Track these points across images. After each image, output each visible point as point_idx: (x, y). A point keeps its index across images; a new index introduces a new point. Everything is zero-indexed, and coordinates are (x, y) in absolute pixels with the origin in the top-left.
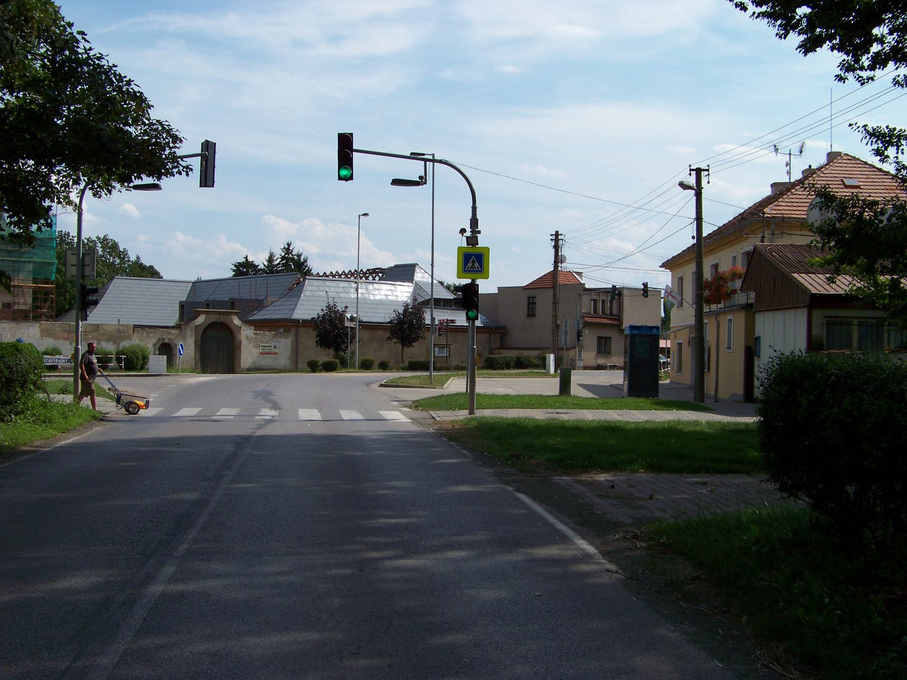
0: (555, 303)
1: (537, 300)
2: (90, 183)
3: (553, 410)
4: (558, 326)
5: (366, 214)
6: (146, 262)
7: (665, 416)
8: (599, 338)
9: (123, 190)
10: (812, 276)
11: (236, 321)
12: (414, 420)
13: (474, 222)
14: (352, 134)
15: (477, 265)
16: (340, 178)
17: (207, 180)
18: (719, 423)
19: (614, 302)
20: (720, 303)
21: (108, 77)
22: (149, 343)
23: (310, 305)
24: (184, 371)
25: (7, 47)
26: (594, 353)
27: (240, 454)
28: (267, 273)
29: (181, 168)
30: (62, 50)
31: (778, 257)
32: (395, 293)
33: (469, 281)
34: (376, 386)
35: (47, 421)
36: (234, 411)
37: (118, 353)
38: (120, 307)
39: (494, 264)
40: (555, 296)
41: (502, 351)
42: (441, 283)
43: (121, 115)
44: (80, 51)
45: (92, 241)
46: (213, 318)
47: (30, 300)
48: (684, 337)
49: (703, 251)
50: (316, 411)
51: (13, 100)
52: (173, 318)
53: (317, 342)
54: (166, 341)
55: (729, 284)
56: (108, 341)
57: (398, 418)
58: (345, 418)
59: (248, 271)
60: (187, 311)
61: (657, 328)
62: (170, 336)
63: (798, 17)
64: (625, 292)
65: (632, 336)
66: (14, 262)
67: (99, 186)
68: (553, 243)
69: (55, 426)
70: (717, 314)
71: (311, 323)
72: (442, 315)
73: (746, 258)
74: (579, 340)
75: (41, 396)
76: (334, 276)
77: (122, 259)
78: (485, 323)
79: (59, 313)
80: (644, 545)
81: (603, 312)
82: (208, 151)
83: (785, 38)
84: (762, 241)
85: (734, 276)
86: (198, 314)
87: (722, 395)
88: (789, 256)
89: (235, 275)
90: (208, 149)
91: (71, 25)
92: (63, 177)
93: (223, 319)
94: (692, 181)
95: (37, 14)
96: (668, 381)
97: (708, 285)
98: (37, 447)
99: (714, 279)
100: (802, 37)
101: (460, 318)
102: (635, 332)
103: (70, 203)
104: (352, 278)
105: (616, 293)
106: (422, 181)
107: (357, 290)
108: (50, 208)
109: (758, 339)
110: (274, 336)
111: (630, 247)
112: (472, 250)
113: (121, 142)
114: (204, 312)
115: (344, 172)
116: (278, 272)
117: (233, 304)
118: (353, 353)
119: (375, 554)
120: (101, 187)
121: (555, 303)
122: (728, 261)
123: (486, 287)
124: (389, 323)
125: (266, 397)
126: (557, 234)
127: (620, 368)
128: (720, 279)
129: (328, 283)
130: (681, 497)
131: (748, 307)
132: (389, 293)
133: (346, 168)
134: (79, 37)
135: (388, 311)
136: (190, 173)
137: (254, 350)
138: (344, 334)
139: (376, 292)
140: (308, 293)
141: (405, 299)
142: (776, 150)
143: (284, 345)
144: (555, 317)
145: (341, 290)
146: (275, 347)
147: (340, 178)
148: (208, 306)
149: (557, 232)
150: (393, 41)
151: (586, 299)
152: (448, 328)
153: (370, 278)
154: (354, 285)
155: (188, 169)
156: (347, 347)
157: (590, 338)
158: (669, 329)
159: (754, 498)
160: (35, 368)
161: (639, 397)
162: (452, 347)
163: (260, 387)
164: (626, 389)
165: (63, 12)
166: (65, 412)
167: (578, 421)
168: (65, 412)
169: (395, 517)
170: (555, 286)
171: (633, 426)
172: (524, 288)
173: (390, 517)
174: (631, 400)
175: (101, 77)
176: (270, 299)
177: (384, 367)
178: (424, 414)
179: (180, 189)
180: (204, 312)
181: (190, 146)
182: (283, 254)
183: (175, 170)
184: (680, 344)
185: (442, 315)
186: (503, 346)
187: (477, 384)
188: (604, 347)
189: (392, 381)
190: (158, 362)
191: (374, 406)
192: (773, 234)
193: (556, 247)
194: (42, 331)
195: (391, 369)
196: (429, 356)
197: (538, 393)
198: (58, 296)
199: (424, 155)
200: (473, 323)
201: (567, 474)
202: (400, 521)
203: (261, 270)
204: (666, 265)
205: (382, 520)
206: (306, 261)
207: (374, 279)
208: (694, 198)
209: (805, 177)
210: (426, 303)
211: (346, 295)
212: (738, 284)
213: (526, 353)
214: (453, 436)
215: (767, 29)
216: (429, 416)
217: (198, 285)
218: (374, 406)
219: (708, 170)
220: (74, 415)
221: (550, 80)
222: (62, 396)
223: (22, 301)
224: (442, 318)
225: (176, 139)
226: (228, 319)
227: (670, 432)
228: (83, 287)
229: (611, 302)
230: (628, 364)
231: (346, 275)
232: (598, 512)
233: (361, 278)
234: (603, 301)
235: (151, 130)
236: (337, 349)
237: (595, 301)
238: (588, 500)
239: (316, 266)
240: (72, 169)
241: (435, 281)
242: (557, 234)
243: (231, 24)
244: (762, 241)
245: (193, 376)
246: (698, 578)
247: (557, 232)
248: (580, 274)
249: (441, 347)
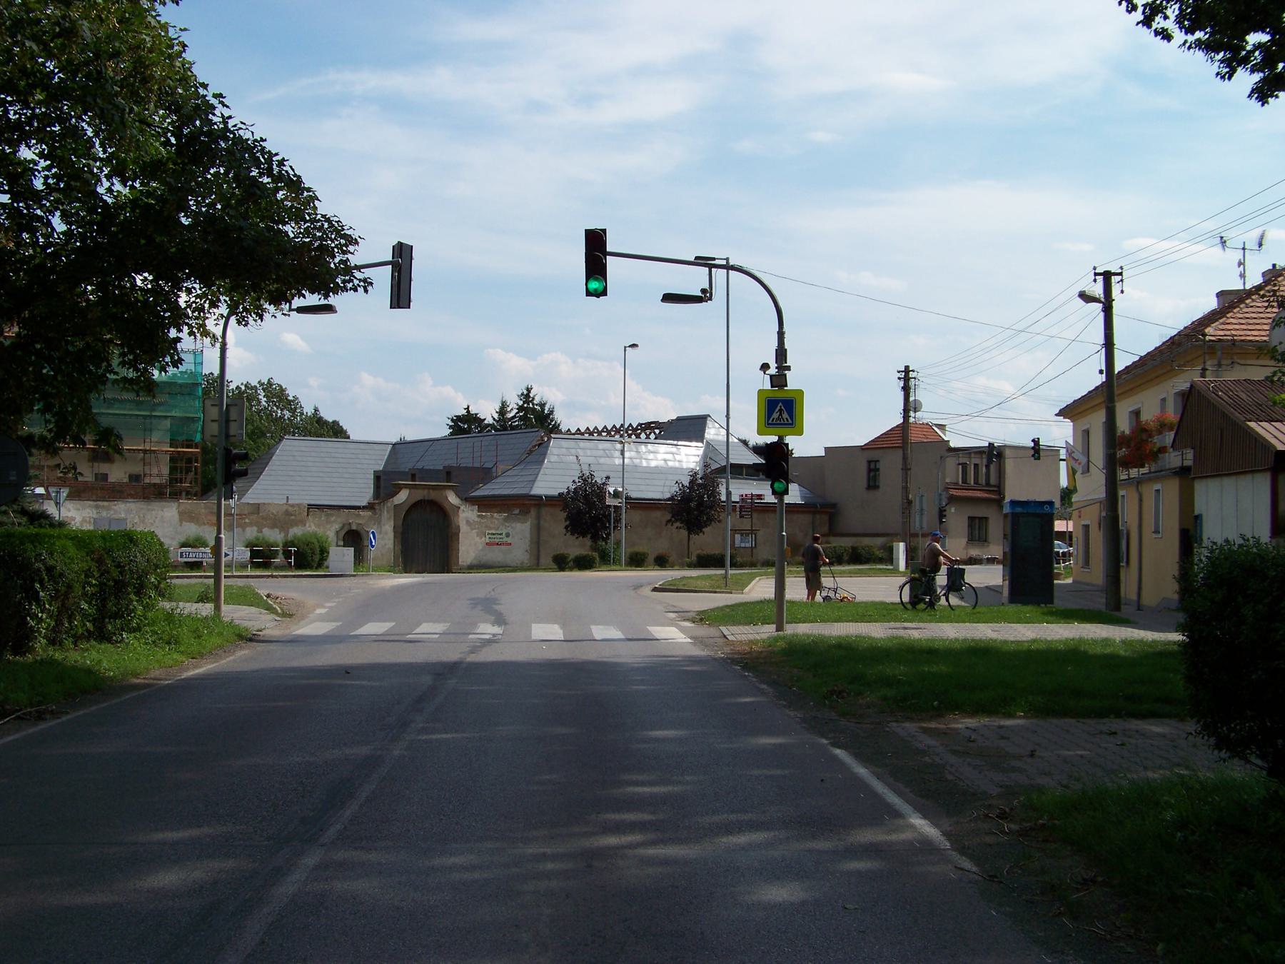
0: (906, 469)
1: (881, 465)
2: (233, 310)
3: (898, 625)
4: (910, 502)
5: (634, 346)
6: (328, 416)
7: (1061, 631)
8: (971, 519)
9: (279, 314)
10: (1277, 424)
11: (453, 499)
12: (697, 640)
13: (781, 354)
14: (604, 231)
15: (785, 415)
16: (589, 293)
17: (400, 297)
18: (1141, 641)
19: (992, 467)
20: (1143, 466)
21: (253, 155)
22: (329, 530)
23: (555, 475)
24: (378, 569)
25: (117, 118)
26: (964, 540)
27: (441, 689)
28: (496, 430)
29: (356, 282)
30: (190, 120)
31: (1226, 398)
32: (678, 457)
33: (775, 439)
34: (647, 591)
35: (173, 641)
36: (439, 628)
37: (286, 544)
38: (289, 480)
39: (810, 414)
40: (905, 458)
41: (832, 539)
42: (745, 443)
43: (278, 214)
44: (215, 119)
45: (252, 388)
46: (420, 495)
47: (166, 471)
48: (1092, 517)
49: (1116, 392)
50: (556, 627)
51: (126, 191)
52: (365, 494)
53: (566, 527)
54: (354, 527)
55: (1156, 439)
56: (273, 526)
57: (674, 636)
58: (598, 637)
59: (469, 427)
60: (384, 484)
61: (1051, 503)
62: (359, 520)
63: (1248, 48)
64: (1008, 453)
65: (1015, 516)
66: (145, 417)
67: (245, 309)
68: (902, 384)
69: (182, 649)
70: (1138, 482)
71: (559, 501)
72: (739, 489)
73: (1180, 401)
74: (941, 522)
75: (167, 605)
76: (591, 434)
77: (293, 411)
78: (785, 502)
79: (205, 490)
80: (1014, 827)
81: (976, 482)
82: (402, 258)
83: (1230, 78)
84: (1203, 375)
85: (1163, 426)
86: (400, 488)
87: (1149, 599)
88: (1243, 396)
89: (452, 434)
90: (402, 254)
91: (205, 86)
92: (197, 297)
93: (433, 495)
94: (1098, 290)
95: (158, 72)
96: (1069, 581)
97: (1125, 441)
98: (155, 679)
99: (1133, 432)
100: (1257, 77)
101: (763, 490)
102: (1019, 510)
103: (206, 333)
104: (617, 437)
105: (994, 454)
106: (705, 296)
107: (622, 453)
108: (178, 340)
109: (1198, 518)
110: (506, 519)
111: (1008, 388)
112: (779, 395)
113: (275, 247)
114: (406, 486)
115: (594, 285)
116: (513, 428)
117: (448, 473)
118: (618, 543)
119: (612, 840)
120: (245, 310)
121: (906, 469)
122: (1155, 404)
123: (803, 446)
124: (669, 499)
125: (489, 608)
126: (907, 370)
127: (999, 562)
128: (1141, 432)
129: (582, 444)
130: (1070, 755)
131: (1183, 472)
132: (669, 457)
133: (596, 279)
134: (214, 101)
135: (668, 483)
136: (369, 288)
137: (477, 539)
138: (604, 516)
139: (651, 456)
140: (553, 458)
141: (692, 466)
142: (1223, 242)
143: (520, 532)
144: (906, 489)
145: (601, 453)
146: (508, 535)
147: (589, 293)
148: (413, 477)
149: (907, 367)
150: (668, 100)
151: (951, 462)
152: (751, 507)
153: (643, 436)
154: (619, 446)
155: (367, 283)
156: (609, 534)
157: (957, 520)
158: (1070, 504)
159: (1169, 755)
160: (157, 566)
161: (1025, 603)
162: (760, 534)
163: (481, 593)
164: (1006, 592)
165: (195, 70)
166: (199, 627)
167: (933, 640)
168: (197, 630)
169: (651, 784)
170: (906, 445)
171: (1013, 647)
172: (862, 448)
173: (643, 784)
174: (1013, 609)
175: (245, 154)
176: (501, 467)
177: (661, 562)
178: (712, 631)
179: (362, 310)
180: (406, 486)
181: (371, 249)
182: (521, 403)
183: (350, 285)
184: (1087, 527)
185: (739, 489)
186: (833, 532)
187: (787, 586)
188: (977, 532)
189: (670, 583)
190: (341, 557)
191: (643, 620)
192: (1219, 365)
193: (906, 389)
194: (180, 513)
195: (672, 566)
196: (725, 549)
197: (877, 599)
198: (205, 463)
199: (714, 259)
200: (781, 500)
201: (910, 719)
202: (656, 789)
203: (489, 425)
204: (1063, 413)
205: (630, 789)
206: (551, 412)
207: (648, 437)
208: (1102, 314)
209: (1266, 283)
210: (722, 470)
211: (607, 461)
212: (1169, 437)
213: (867, 541)
214: (751, 663)
215: (1204, 66)
216: (718, 634)
217: (400, 447)
218: (643, 620)
219: (1120, 274)
220: (210, 633)
221: (885, 153)
222: (196, 605)
223: (155, 471)
224: (744, 492)
225: (352, 241)
226: (437, 498)
227: (1073, 655)
228: (228, 451)
229: (987, 467)
230: (1009, 556)
231: (609, 432)
232: (950, 777)
233: (630, 436)
234: (976, 465)
235: (315, 228)
236: (595, 538)
237: (964, 466)
238: (937, 759)
239: (565, 419)
240: (209, 286)
241: (733, 440)
242: (907, 370)
243: (440, 82)
244: (1203, 375)
245: (388, 577)
246: (1093, 881)
247: (907, 367)
248: (942, 427)
249: (744, 533)
